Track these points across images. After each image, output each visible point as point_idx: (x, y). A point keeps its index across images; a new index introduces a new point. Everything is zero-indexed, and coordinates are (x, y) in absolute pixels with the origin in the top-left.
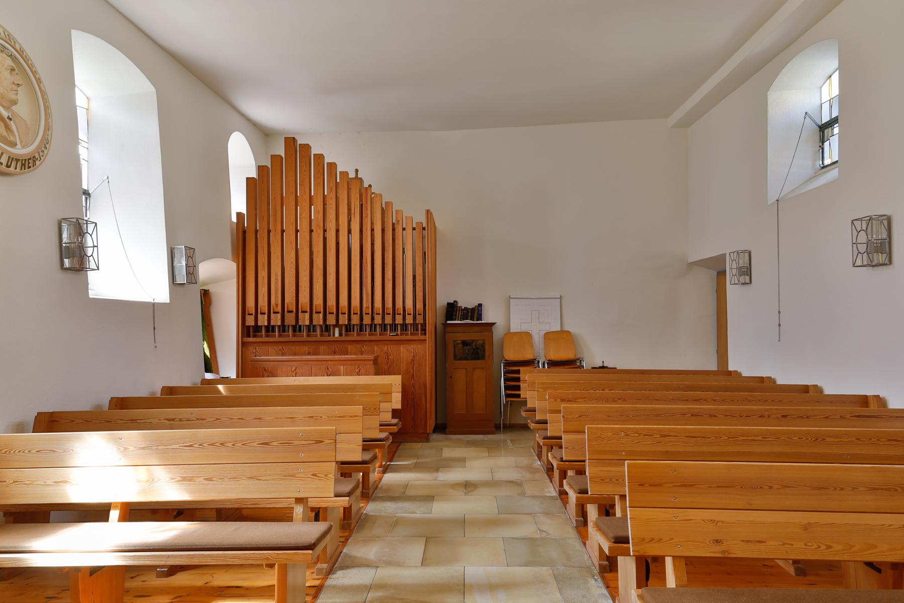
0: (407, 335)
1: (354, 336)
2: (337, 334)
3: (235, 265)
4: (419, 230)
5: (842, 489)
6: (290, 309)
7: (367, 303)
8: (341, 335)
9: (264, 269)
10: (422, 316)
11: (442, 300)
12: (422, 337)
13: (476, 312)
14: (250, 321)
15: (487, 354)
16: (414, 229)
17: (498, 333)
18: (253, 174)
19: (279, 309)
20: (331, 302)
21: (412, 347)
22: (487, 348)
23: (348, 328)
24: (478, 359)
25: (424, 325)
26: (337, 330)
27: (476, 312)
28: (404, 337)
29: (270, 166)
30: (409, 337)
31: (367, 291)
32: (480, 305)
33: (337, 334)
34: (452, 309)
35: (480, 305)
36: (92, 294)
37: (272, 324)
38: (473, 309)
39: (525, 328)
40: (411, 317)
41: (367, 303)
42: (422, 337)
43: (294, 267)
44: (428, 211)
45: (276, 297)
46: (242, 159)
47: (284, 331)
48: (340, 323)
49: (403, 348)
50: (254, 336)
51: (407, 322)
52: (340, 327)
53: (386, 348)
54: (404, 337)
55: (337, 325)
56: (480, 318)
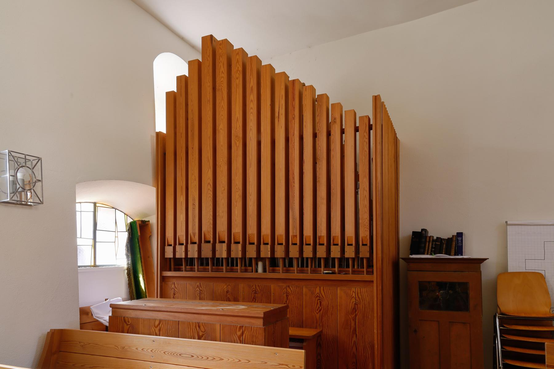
0: (347, 273)
1: (295, 274)
2: (260, 269)
3: (154, 190)
4: (364, 129)
5: (335, 119)
6: (238, 241)
7: (294, 231)
8: (264, 270)
9: (182, 194)
10: (367, 248)
11: (406, 229)
12: (366, 277)
13: (455, 243)
14: (169, 253)
15: (472, 303)
16: (357, 129)
17: (489, 271)
18: (173, 88)
19: (196, 239)
20: (252, 230)
21: (354, 290)
22: (471, 294)
23: (273, 262)
24: (459, 309)
25: (370, 260)
26: (260, 264)
27: (455, 243)
28: (342, 277)
29: (187, 75)
30: (350, 277)
31: (293, 215)
32: (460, 235)
33: (260, 269)
34: (419, 239)
35: (460, 235)
36: (509, 271)
37: (217, 256)
38: (449, 240)
39: (532, 267)
40: (353, 248)
41: (294, 231)
42: (366, 277)
43: (211, 189)
44: (376, 99)
45: (194, 225)
46: (168, 71)
47: (218, 265)
48: (262, 255)
49: (340, 291)
50: (175, 270)
51: (347, 255)
52: (263, 260)
53: (318, 290)
54: (342, 277)
55: (259, 258)
56: (459, 251)
